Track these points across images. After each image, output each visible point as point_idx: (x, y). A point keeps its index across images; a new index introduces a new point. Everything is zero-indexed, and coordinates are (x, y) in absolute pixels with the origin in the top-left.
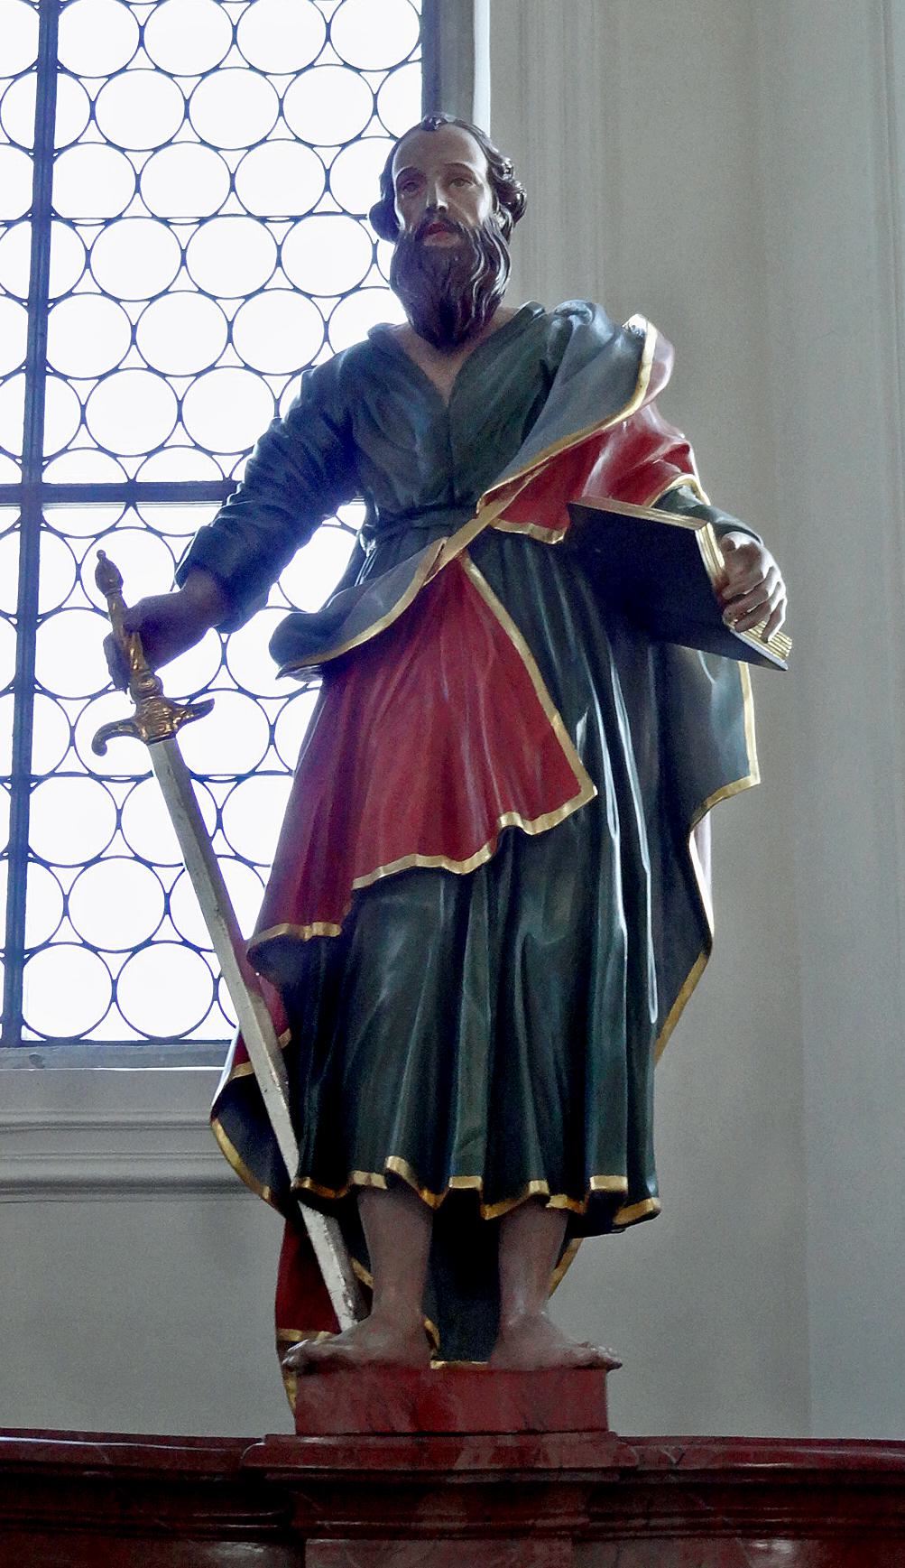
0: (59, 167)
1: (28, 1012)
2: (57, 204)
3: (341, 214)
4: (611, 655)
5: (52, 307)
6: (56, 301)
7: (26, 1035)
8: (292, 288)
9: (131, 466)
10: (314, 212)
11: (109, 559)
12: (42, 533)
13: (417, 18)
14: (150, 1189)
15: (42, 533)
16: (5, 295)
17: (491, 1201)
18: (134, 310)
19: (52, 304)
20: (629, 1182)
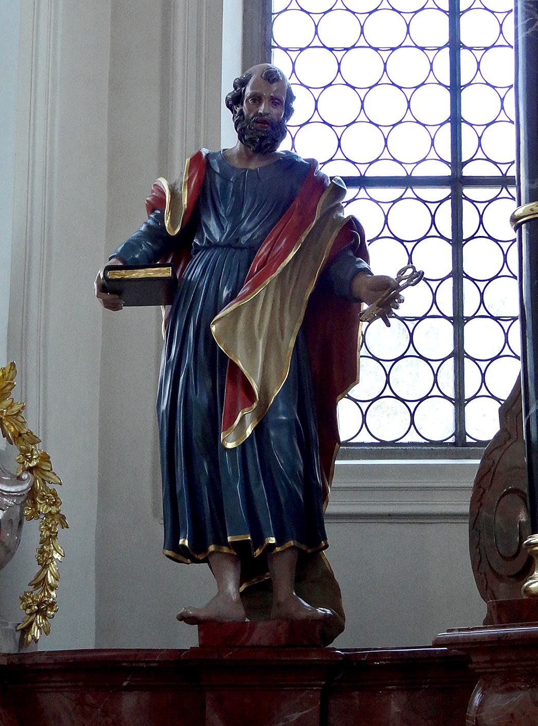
0: (447, 114)
1: (468, 430)
2: (449, 248)
3: (322, 47)
4: (269, 242)
5: (463, 89)
6: (464, 12)
7: (468, 440)
8: (431, 62)
9: (409, 168)
10: (355, 46)
11: (448, 38)
12: (449, 85)
13: (424, 46)
14: (417, 517)
15: (449, 85)
16: (325, 89)
17: (278, 546)
18: (362, 93)
19: (463, 87)
20: (227, 539)
